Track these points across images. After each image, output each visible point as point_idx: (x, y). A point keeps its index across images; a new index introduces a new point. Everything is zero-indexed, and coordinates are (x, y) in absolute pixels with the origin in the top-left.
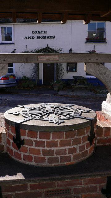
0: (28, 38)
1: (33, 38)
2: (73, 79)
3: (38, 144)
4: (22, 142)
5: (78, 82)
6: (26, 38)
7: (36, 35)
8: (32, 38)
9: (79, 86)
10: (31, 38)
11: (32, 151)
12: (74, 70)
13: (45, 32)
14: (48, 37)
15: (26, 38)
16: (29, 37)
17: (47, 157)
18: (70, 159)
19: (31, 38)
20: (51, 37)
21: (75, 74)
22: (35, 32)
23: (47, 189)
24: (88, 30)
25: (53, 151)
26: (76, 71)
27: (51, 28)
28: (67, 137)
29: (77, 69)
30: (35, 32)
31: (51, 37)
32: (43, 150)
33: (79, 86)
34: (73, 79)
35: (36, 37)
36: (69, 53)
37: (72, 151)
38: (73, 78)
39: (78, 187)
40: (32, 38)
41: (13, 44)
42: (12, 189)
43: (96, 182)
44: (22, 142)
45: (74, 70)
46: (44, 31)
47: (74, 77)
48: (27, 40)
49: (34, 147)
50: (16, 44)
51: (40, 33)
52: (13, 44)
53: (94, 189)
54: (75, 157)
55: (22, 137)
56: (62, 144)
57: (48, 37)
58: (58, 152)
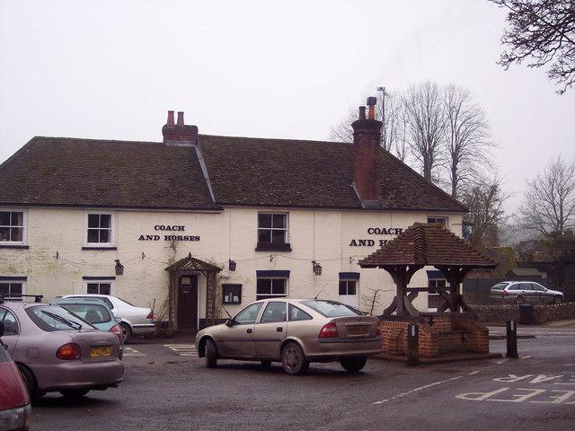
0: (358, 243)
1: (157, 238)
6: (142, 238)
7: (162, 234)
8: (369, 245)
10: (367, 243)
12: (236, 298)
13: (181, 228)
14: (186, 238)
15: (142, 238)
16: (148, 236)
18: (17, 405)
19: (367, 243)
20: (192, 238)
22: (162, 228)
24: (260, 225)
27: (193, 224)
30: (162, 228)
31: (192, 238)
35: (162, 238)
40: (369, 245)
41: (115, 249)
46: (396, 230)
48: (357, 248)
50: (119, 250)
51: (386, 233)
52: (115, 249)
57: (186, 238)
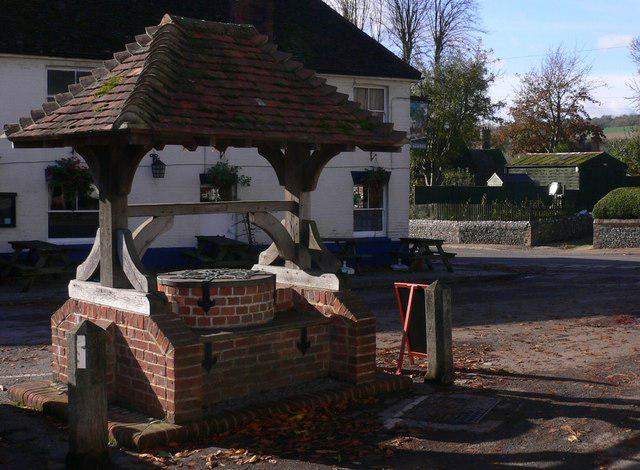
2: (13, 251)
3: (233, 301)
4: (213, 303)
5: (42, 260)
9: (46, 271)
11: (225, 311)
12: (8, 221)
17: (241, 316)
21: (12, 235)
23: (251, 346)
25: (246, 308)
26: (13, 225)
28: (260, 291)
29: (19, 218)
32: (238, 308)
33: (46, 271)
34: (13, 251)
36: (194, 198)
37: (263, 307)
38: (10, 250)
39: (277, 341)
42: (221, 347)
43: (292, 335)
44: (213, 303)
45: (8, 221)
47: (15, 245)
49: (227, 306)
53: (289, 345)
54: (266, 315)
55: (212, 298)
56: (257, 299)
58: (253, 309)
